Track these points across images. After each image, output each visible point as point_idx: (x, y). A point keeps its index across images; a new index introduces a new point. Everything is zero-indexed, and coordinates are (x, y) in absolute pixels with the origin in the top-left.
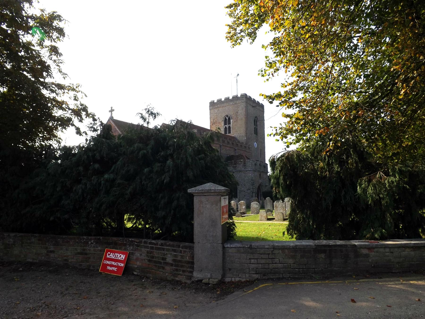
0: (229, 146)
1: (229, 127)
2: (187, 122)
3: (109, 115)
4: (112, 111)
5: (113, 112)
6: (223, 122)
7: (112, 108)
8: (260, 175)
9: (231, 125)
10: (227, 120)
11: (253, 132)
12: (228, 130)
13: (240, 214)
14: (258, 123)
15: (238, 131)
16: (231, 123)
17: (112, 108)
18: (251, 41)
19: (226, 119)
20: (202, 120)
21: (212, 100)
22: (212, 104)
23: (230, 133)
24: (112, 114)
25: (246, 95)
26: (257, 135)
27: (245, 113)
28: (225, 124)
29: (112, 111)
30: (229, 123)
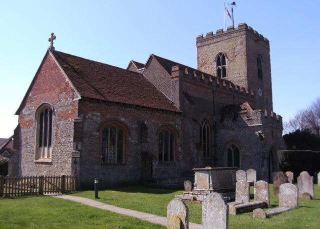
0: (225, 91)
1: (224, 69)
2: (124, 66)
3: (49, 44)
4: (53, 38)
5: (54, 41)
6: (215, 63)
7: (53, 34)
8: (272, 132)
9: (227, 66)
10: (221, 59)
11: (257, 75)
12: (222, 72)
13: (46, 98)
14: (262, 63)
15: (238, 73)
16: (227, 63)
17: (53, 34)
18: (182, 76)
19: (219, 58)
20: (187, 57)
21: (200, 34)
22: (201, 40)
23: (225, 75)
24: (52, 43)
25: (246, 25)
26: (261, 78)
27: (245, 48)
28: (218, 64)
29: (53, 38)
30: (224, 63)
